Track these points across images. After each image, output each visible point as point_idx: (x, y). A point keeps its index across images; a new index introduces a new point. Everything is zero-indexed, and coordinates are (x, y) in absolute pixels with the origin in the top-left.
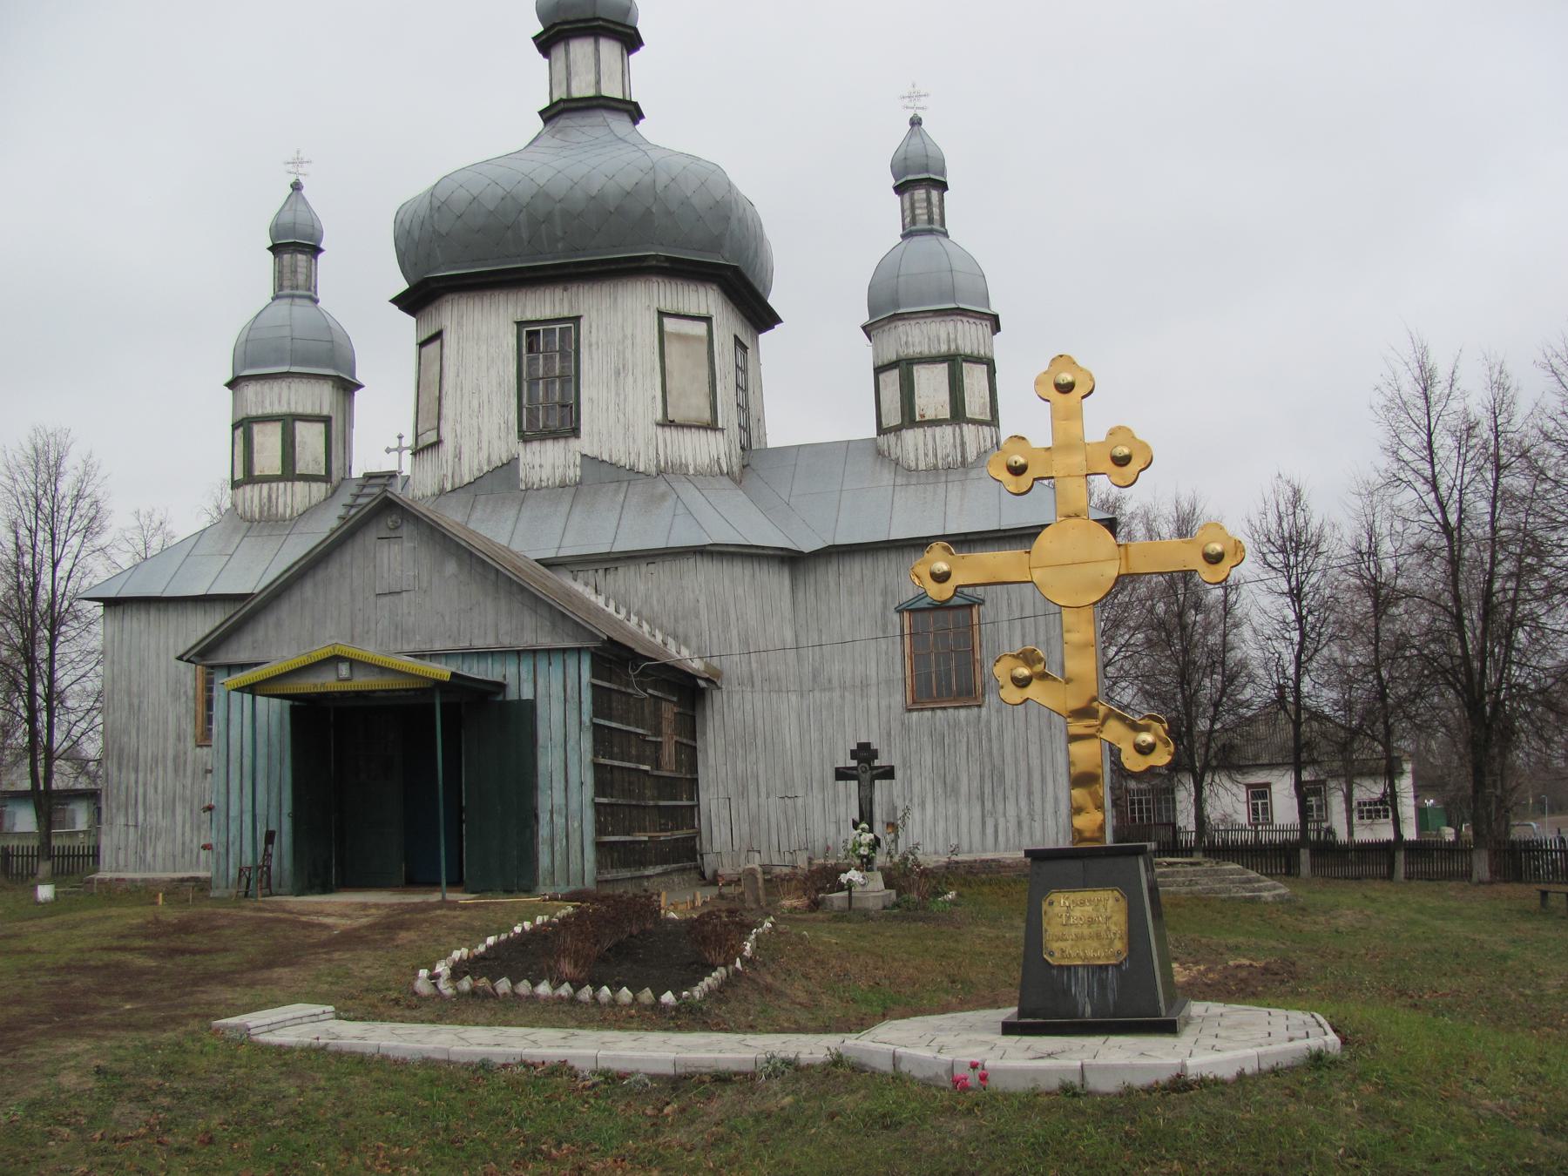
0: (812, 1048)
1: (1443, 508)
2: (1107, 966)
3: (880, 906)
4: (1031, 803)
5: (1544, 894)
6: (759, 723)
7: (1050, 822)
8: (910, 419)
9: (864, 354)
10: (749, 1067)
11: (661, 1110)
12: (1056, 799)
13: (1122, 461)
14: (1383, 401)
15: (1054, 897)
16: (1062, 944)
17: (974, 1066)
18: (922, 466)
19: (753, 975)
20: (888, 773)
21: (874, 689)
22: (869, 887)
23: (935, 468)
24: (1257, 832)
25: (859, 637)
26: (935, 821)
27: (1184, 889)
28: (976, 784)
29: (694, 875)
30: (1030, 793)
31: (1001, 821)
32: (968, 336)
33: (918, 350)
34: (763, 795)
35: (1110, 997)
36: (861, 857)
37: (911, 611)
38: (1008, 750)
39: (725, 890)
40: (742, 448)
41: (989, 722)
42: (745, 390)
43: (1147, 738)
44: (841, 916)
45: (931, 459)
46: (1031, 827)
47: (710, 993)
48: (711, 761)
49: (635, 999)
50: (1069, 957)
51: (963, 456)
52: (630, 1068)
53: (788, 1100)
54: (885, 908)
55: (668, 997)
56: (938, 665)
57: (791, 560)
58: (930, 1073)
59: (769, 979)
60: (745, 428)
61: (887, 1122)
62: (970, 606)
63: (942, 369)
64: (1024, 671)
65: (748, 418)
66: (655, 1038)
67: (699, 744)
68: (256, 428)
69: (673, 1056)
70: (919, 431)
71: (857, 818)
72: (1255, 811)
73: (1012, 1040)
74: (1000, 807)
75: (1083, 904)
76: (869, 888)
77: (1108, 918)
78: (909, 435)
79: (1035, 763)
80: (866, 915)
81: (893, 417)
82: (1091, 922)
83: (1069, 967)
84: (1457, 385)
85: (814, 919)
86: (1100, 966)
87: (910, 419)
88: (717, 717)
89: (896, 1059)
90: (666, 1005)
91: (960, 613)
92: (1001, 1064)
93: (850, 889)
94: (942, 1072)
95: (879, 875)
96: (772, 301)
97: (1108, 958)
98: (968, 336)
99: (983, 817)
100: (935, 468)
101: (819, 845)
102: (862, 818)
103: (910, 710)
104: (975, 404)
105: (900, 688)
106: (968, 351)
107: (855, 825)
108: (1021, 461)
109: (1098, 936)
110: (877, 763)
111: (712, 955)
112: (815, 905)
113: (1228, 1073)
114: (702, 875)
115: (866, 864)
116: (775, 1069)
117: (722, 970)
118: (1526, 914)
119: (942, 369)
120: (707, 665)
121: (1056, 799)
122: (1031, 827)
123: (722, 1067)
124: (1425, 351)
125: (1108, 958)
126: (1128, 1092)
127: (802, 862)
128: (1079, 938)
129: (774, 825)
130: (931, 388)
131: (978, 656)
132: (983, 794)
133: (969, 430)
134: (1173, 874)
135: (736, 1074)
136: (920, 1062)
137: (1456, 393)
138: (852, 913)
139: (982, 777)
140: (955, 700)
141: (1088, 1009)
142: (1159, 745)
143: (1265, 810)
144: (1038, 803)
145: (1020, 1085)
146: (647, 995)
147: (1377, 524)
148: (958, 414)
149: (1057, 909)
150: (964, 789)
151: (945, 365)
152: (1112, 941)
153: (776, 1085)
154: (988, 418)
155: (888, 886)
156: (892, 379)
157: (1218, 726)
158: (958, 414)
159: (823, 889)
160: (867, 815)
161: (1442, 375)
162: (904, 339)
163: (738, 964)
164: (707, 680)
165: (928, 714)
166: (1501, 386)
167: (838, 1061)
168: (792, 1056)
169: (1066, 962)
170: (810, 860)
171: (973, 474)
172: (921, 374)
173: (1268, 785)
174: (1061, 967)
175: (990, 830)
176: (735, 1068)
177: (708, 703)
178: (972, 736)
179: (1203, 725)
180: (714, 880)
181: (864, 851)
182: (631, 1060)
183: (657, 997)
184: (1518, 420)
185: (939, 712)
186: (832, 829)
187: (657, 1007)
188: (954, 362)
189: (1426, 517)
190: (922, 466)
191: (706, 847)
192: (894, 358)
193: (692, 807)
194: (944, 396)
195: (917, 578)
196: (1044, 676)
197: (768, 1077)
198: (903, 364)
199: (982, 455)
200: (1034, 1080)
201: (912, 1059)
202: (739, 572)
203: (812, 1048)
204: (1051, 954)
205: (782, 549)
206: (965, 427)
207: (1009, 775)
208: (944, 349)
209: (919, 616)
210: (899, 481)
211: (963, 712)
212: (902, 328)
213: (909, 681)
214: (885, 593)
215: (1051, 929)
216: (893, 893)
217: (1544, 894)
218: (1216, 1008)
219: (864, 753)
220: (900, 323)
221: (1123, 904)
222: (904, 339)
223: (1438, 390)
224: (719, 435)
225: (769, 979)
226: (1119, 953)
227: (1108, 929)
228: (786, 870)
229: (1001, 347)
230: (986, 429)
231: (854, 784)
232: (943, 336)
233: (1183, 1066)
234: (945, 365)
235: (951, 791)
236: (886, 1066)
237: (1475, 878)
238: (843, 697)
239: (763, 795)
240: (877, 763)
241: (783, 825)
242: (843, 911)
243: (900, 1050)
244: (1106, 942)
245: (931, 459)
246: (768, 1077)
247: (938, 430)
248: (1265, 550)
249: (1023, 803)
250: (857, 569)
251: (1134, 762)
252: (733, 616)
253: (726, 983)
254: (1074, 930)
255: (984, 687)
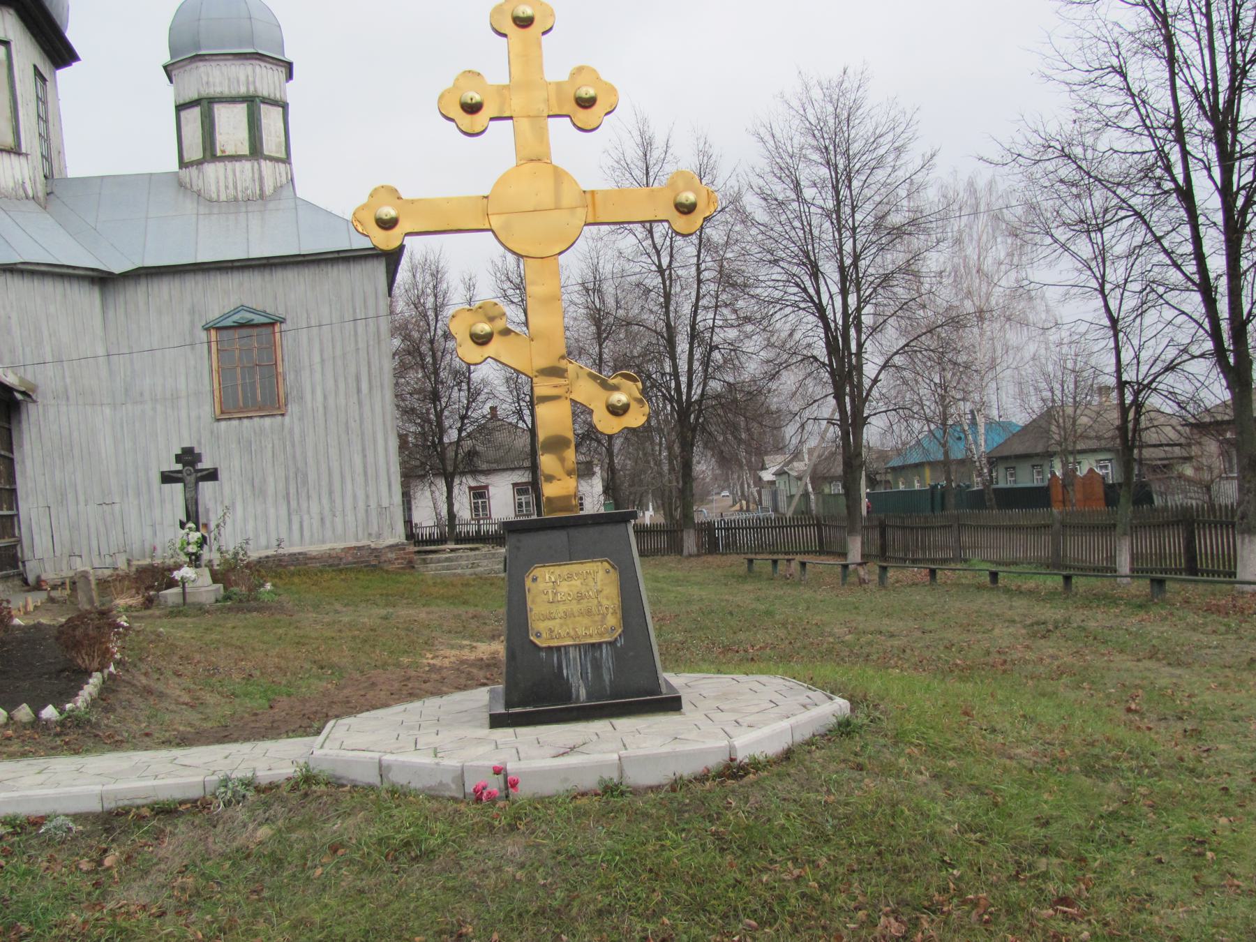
0: (274, 759)
1: (658, 253)
2: (600, 644)
3: (213, 600)
4: (332, 501)
5: (751, 561)
6: (75, 434)
7: (350, 518)
8: (211, 153)
9: (167, 95)
10: (196, 793)
11: (100, 863)
12: (355, 497)
13: (586, 103)
14: (611, 163)
15: (538, 572)
16: (550, 624)
17: (497, 771)
18: (223, 198)
19: (127, 677)
20: (212, 475)
21: (183, 403)
22: (198, 582)
23: (236, 200)
24: (479, 526)
25: (168, 350)
26: (245, 520)
27: (468, 571)
28: (281, 485)
29: (17, 582)
30: (331, 493)
31: (306, 517)
32: (265, 80)
33: (218, 90)
34: (82, 503)
35: (606, 678)
36: (189, 555)
37: (218, 329)
38: (310, 454)
39: (54, 594)
40: (45, 177)
41: (291, 431)
42: (46, 121)
43: (619, 398)
44: (176, 612)
45: (231, 192)
46: (333, 522)
47: (93, 703)
48: (29, 472)
49: (10, 718)
50: (559, 637)
51: (261, 189)
52: (43, 810)
53: (264, 832)
54: (217, 601)
55: (50, 712)
56: (243, 378)
57: (102, 280)
58: (432, 782)
59: (144, 681)
60: (46, 158)
61: (409, 851)
62: (272, 324)
63: (242, 109)
64: (484, 328)
65: (49, 148)
66: (63, 765)
67: (17, 456)
68: (186, 159)
69: (98, 789)
70: (220, 165)
71: (185, 520)
72: (476, 509)
73: (505, 735)
74: (304, 505)
75: (570, 577)
76: (199, 583)
77: (599, 592)
78: (211, 169)
79: (335, 465)
80: (201, 609)
81: (194, 151)
82: (580, 597)
83: (558, 648)
84: (670, 151)
85: (151, 616)
86: (593, 645)
87: (211, 153)
88: (34, 430)
89: (383, 769)
90: (47, 721)
91: (264, 330)
92: (525, 765)
93: (184, 584)
94: (447, 779)
95: (206, 571)
96: (72, 35)
97: (601, 635)
98: (265, 80)
99: (289, 514)
100: (236, 200)
101: (136, 547)
102: (189, 518)
103: (218, 420)
104: (271, 144)
105: (209, 399)
106: (265, 94)
107: (182, 525)
108: (477, 98)
109: (589, 612)
110: (200, 466)
111: (82, 661)
112: (149, 603)
113: (774, 748)
114: (25, 582)
115: (195, 560)
116: (235, 793)
117: (98, 674)
118: (742, 579)
119: (242, 109)
120: (22, 380)
121: (355, 497)
122: (333, 522)
123: (163, 796)
124: (645, 120)
125: (601, 635)
126: (677, 785)
127: (122, 564)
128: (567, 615)
129: (93, 530)
130: (231, 126)
131: (280, 370)
132: (288, 494)
133: (266, 166)
134: (457, 559)
135: (181, 803)
136: (417, 770)
137: (669, 157)
138: (185, 609)
139: (287, 479)
140: (260, 409)
141: (583, 693)
142: (634, 405)
143: (484, 508)
144: (338, 501)
145: (551, 787)
146: (24, 712)
147: (601, 265)
148: (256, 150)
149: (541, 585)
150: (271, 490)
151: (244, 106)
152: (604, 616)
153: (241, 813)
154: (283, 156)
155: (215, 581)
156: (193, 117)
157: (464, 434)
158: (256, 150)
159: (151, 587)
160: (192, 514)
161: (659, 143)
162: (205, 79)
163: (112, 669)
164: (23, 393)
165: (235, 423)
166: (704, 153)
167: (307, 780)
168: (250, 775)
169: (554, 643)
170: (129, 562)
171: (271, 205)
172: (221, 112)
173: (486, 487)
174: (550, 648)
175: (296, 526)
176: (179, 795)
177: (24, 416)
178: (276, 442)
179: (452, 435)
180: (38, 586)
181: (192, 549)
182: (44, 800)
183: (37, 712)
184: (719, 182)
185: (246, 422)
186: (148, 532)
187: (37, 723)
188: (252, 102)
189: (644, 258)
190: (223, 198)
191: (28, 554)
192: (195, 97)
193: (12, 516)
194: (243, 134)
195: (222, 298)
196: (506, 332)
197: (228, 804)
198: (205, 103)
199: (278, 189)
200: (566, 780)
201: (404, 766)
202: (51, 289)
203: (274, 759)
204: (538, 635)
205: (93, 270)
206: (263, 163)
207: (312, 476)
208: (243, 90)
209: (225, 333)
210: (202, 210)
211: (268, 421)
212: (203, 68)
213: (217, 393)
214: (192, 311)
215: (537, 606)
216: (221, 586)
217: (751, 561)
218: (722, 682)
219: (188, 457)
220: (201, 64)
221: (614, 575)
222: (205, 79)
223: (656, 154)
224: (23, 159)
225: (144, 681)
226: (613, 629)
227: (600, 604)
228: (107, 572)
229: (292, 92)
230: (282, 166)
231: (180, 486)
232: (242, 78)
233: (732, 748)
234: (244, 106)
235: (259, 492)
236: (373, 778)
237: (685, 552)
238: (154, 409)
239: (82, 503)
240: (200, 466)
241: (102, 530)
242: (178, 606)
243: (388, 758)
244: (597, 618)
245: (231, 192)
246: (228, 804)
247: (238, 165)
248: (505, 287)
249: (325, 501)
250: (165, 289)
251: (607, 424)
252: (46, 333)
253: (107, 689)
254: (562, 608)
255: (286, 398)
